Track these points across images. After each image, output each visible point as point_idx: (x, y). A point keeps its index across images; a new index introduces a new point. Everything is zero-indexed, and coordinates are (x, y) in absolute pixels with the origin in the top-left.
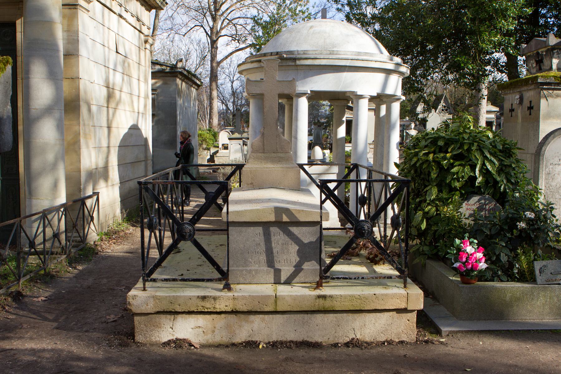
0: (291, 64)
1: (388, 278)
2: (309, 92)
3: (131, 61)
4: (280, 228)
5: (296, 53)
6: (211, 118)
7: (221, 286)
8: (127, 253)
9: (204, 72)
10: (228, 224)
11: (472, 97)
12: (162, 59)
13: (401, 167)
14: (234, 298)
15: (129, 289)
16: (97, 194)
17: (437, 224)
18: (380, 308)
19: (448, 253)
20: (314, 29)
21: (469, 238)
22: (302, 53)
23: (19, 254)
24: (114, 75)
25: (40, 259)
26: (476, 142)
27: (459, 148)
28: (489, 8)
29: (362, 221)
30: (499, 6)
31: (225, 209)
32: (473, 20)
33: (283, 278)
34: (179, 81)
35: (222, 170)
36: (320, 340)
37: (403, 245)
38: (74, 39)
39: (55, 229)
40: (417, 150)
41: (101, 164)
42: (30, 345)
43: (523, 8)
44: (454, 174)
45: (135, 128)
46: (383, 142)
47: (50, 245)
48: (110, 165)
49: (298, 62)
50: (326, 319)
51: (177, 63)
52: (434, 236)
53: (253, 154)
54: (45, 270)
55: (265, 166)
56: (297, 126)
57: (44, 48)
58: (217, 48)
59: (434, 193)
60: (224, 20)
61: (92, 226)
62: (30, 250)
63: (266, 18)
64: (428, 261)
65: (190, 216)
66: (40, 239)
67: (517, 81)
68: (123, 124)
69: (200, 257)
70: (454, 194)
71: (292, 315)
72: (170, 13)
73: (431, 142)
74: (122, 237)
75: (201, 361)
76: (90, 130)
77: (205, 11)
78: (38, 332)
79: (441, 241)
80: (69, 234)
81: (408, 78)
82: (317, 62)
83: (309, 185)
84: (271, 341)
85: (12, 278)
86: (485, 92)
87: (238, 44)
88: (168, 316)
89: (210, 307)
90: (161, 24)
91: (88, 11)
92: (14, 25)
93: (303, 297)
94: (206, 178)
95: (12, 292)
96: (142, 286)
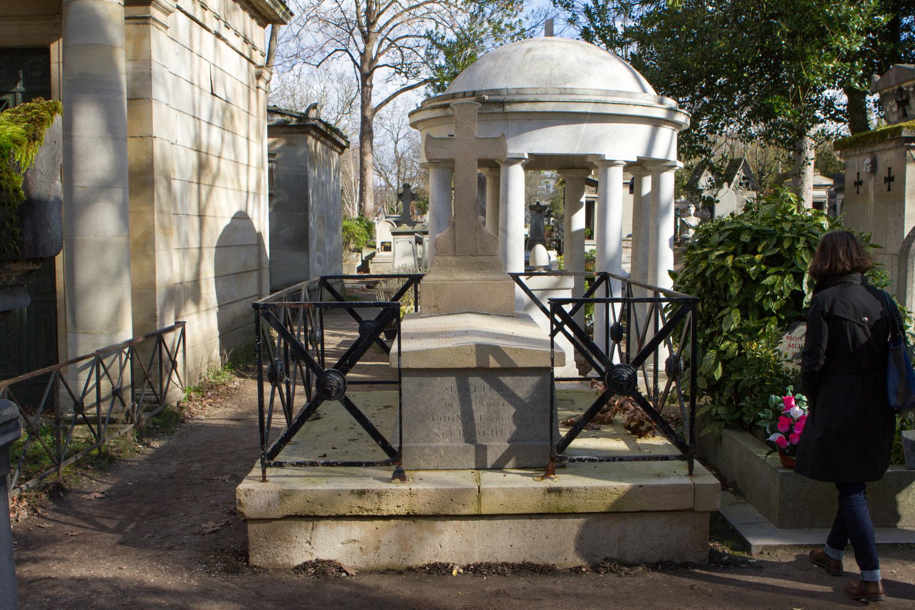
0: (496, 110)
1: (608, 460)
2: (526, 156)
3: (234, 108)
4: (484, 377)
5: (505, 93)
6: (362, 199)
7: (389, 474)
8: (231, 420)
9: (350, 125)
10: (401, 372)
11: (790, 161)
12: (282, 105)
13: (679, 278)
14: (411, 494)
15: (239, 481)
16: (183, 324)
17: (740, 370)
19: (760, 418)
20: (533, 53)
21: (794, 393)
22: (514, 92)
23: (58, 422)
24: (209, 131)
25: (93, 430)
26: (802, 235)
27: (775, 246)
28: (819, 16)
29: (618, 366)
30: (836, 12)
31: (394, 348)
32: (792, 37)
33: (491, 461)
34: (311, 140)
35: (384, 285)
36: (551, 562)
37: (686, 404)
38: (143, 74)
39: (115, 381)
40: (706, 250)
41: (188, 276)
42: (78, 572)
43: (874, 15)
44: (767, 288)
45: (241, 217)
46: (648, 238)
47: (108, 407)
48: (203, 277)
49: (508, 108)
50: (561, 527)
51: (308, 111)
52: (736, 390)
53: (437, 258)
54: (100, 448)
55: (458, 277)
56: (506, 212)
57: (95, 85)
58: (371, 86)
59: (734, 320)
60: (382, 41)
61: (174, 377)
62: (76, 416)
63: (451, 36)
64: (725, 431)
65: (334, 361)
66: (91, 398)
67: (867, 136)
68: (224, 208)
69: (352, 426)
70: (768, 321)
71: (506, 521)
72: (296, 29)
73: (728, 237)
74: (223, 393)
75: (357, 596)
76: (170, 221)
77: (351, 26)
78: (90, 549)
79: (747, 398)
80: (138, 391)
81: (688, 131)
82: (539, 107)
83: (528, 307)
84: (471, 563)
85: (47, 462)
86: (811, 154)
87: (405, 79)
88: (304, 523)
89: (372, 507)
90: (280, 48)
91: (167, 28)
92: (46, 52)
93: (526, 491)
94: (356, 298)
95: (47, 485)
96: (260, 473)
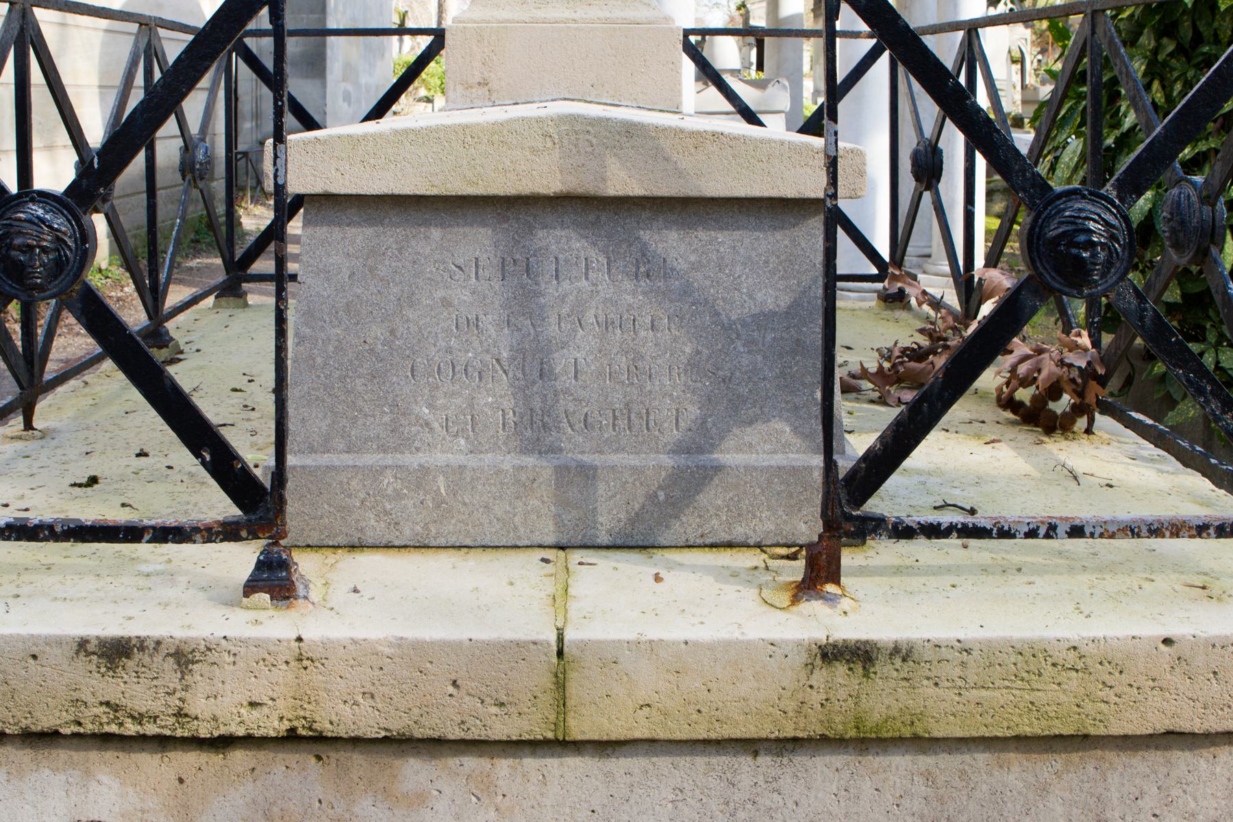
14: (303, 656)
18: (1197, 727)
50: (867, 786)
89: (156, 707)
93: (732, 654)
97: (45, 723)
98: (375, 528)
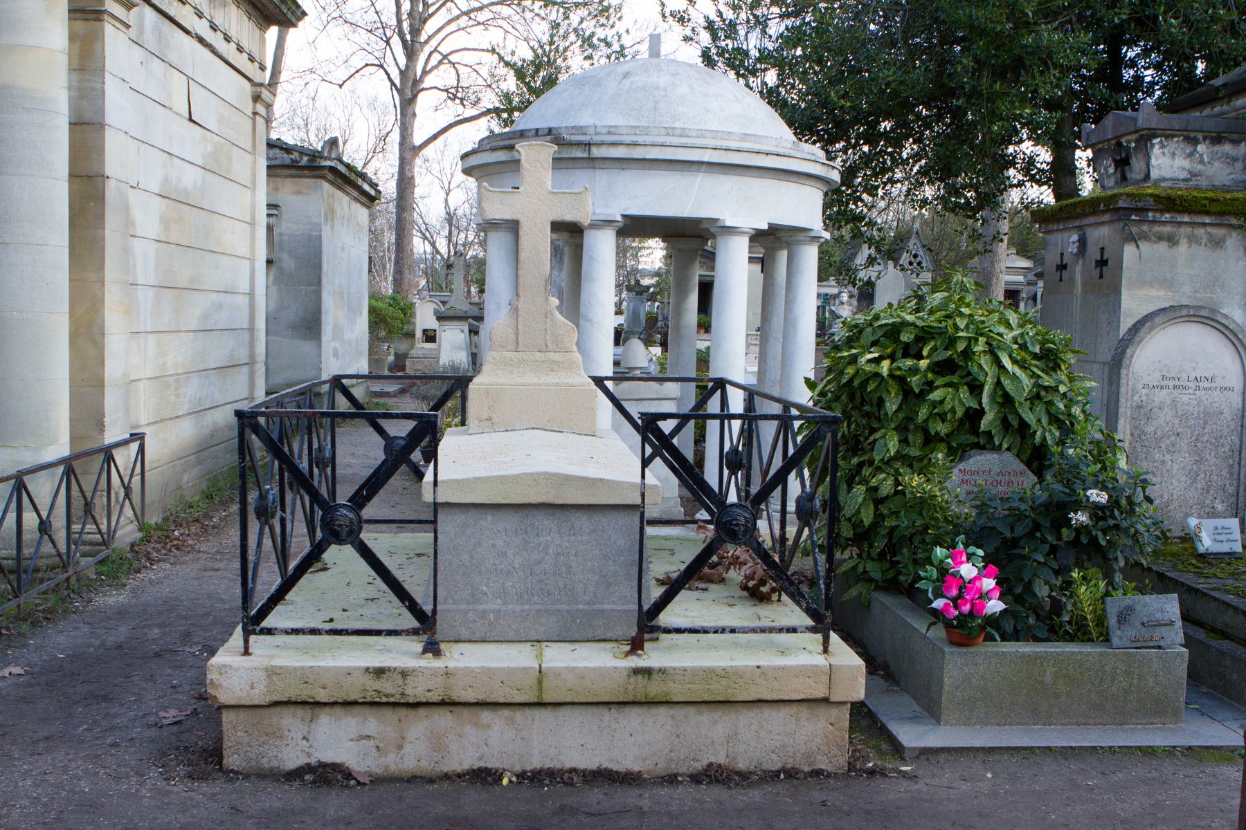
14: (448, 673)
18: (769, 698)
93: (603, 672)
97: (353, 697)
98: (465, 634)
